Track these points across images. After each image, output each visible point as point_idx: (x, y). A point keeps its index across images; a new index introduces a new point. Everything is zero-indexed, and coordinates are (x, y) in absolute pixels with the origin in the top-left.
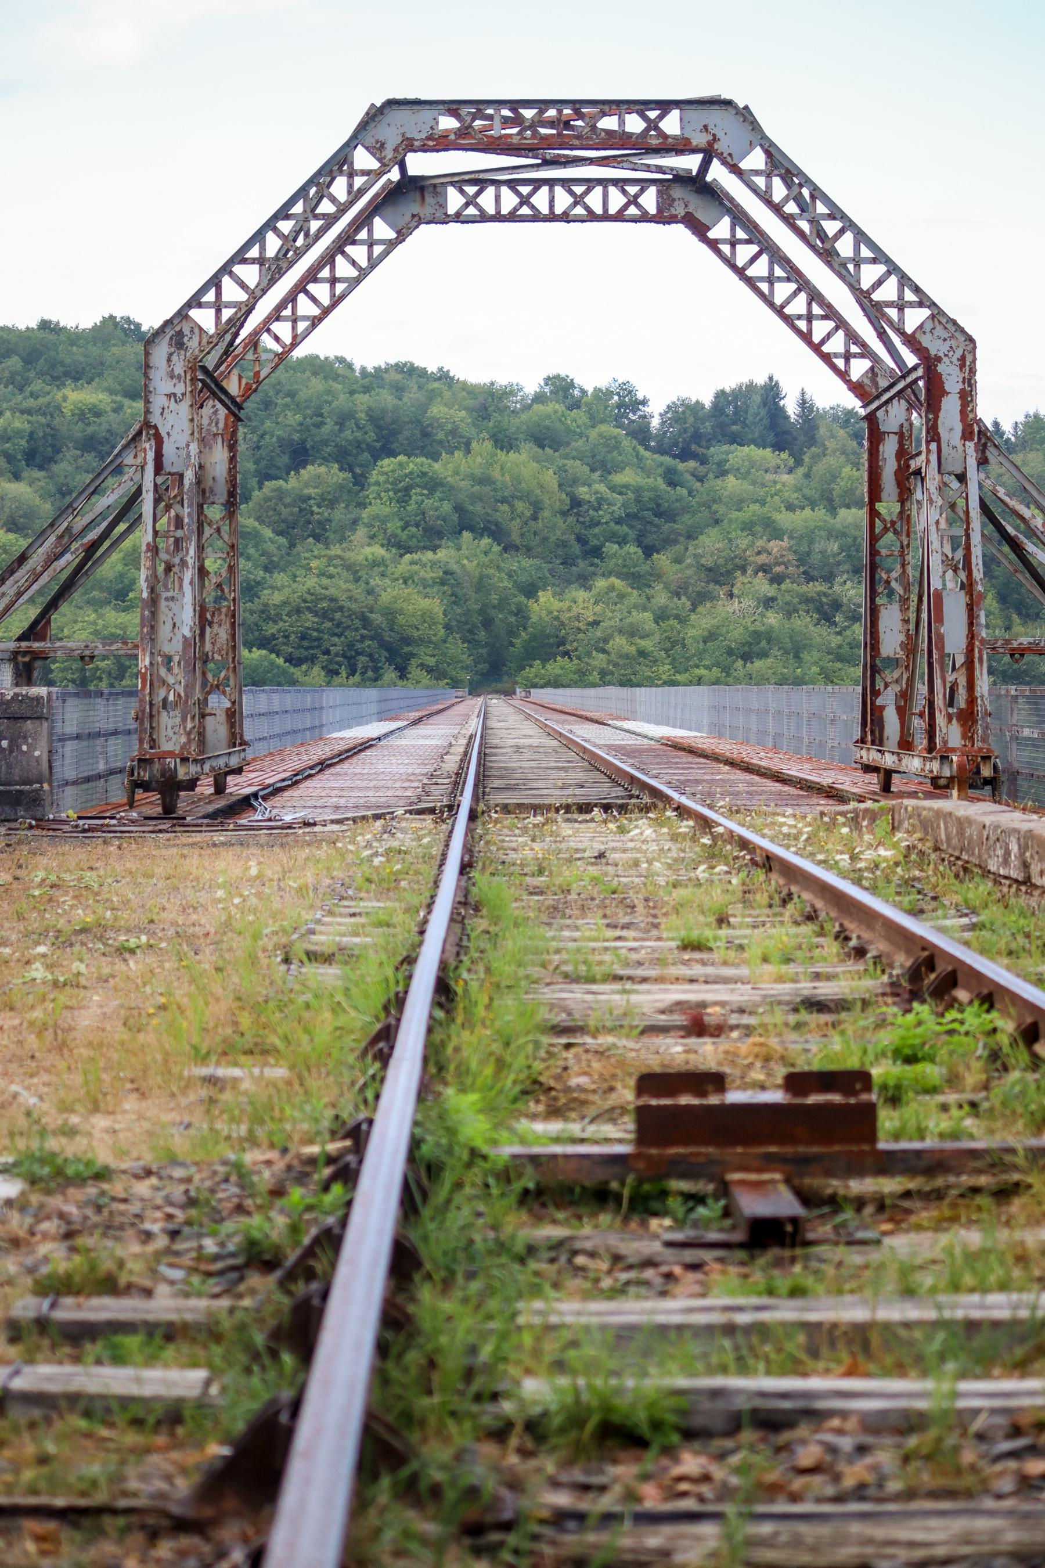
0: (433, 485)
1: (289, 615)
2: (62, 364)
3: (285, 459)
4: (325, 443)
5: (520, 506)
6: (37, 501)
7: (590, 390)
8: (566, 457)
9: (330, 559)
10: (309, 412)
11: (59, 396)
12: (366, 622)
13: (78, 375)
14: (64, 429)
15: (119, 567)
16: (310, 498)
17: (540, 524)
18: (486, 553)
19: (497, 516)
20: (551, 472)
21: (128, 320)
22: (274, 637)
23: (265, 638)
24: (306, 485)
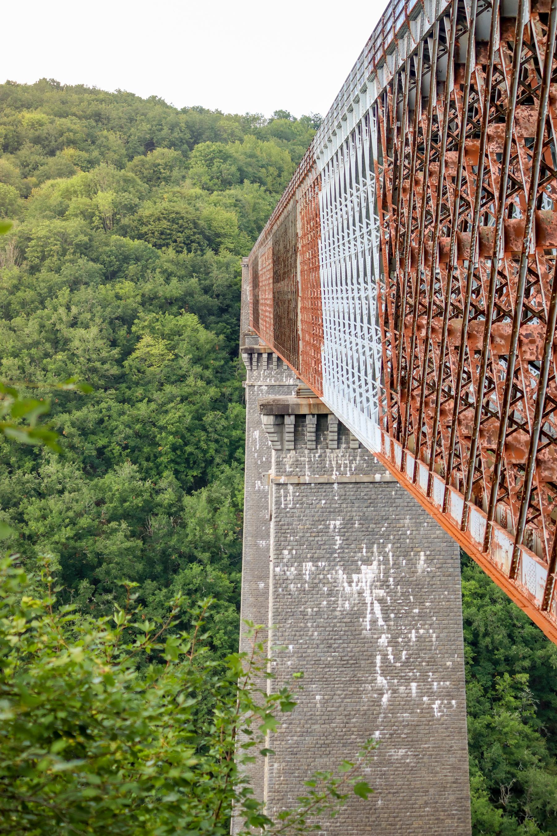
0: (225, 157)
1: (154, 221)
2: (20, 100)
3: (142, 149)
4: (163, 139)
5: (271, 169)
6: (12, 168)
7: (299, 117)
8: (294, 144)
9: (174, 193)
10: (154, 123)
11: (20, 116)
12: (196, 225)
13: (28, 106)
14: (24, 133)
15: (60, 199)
16: (159, 165)
17: (282, 180)
18: (257, 191)
19: (260, 174)
20: (287, 152)
21: (53, 81)
22: (146, 233)
23: (141, 234)
24: (157, 158)
